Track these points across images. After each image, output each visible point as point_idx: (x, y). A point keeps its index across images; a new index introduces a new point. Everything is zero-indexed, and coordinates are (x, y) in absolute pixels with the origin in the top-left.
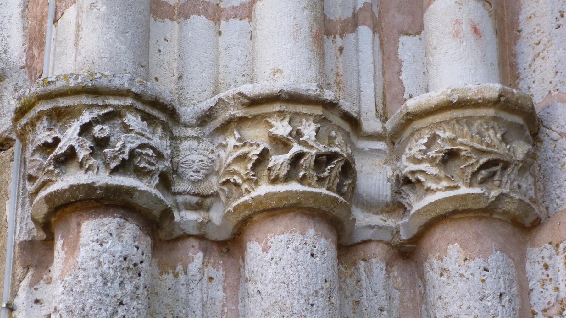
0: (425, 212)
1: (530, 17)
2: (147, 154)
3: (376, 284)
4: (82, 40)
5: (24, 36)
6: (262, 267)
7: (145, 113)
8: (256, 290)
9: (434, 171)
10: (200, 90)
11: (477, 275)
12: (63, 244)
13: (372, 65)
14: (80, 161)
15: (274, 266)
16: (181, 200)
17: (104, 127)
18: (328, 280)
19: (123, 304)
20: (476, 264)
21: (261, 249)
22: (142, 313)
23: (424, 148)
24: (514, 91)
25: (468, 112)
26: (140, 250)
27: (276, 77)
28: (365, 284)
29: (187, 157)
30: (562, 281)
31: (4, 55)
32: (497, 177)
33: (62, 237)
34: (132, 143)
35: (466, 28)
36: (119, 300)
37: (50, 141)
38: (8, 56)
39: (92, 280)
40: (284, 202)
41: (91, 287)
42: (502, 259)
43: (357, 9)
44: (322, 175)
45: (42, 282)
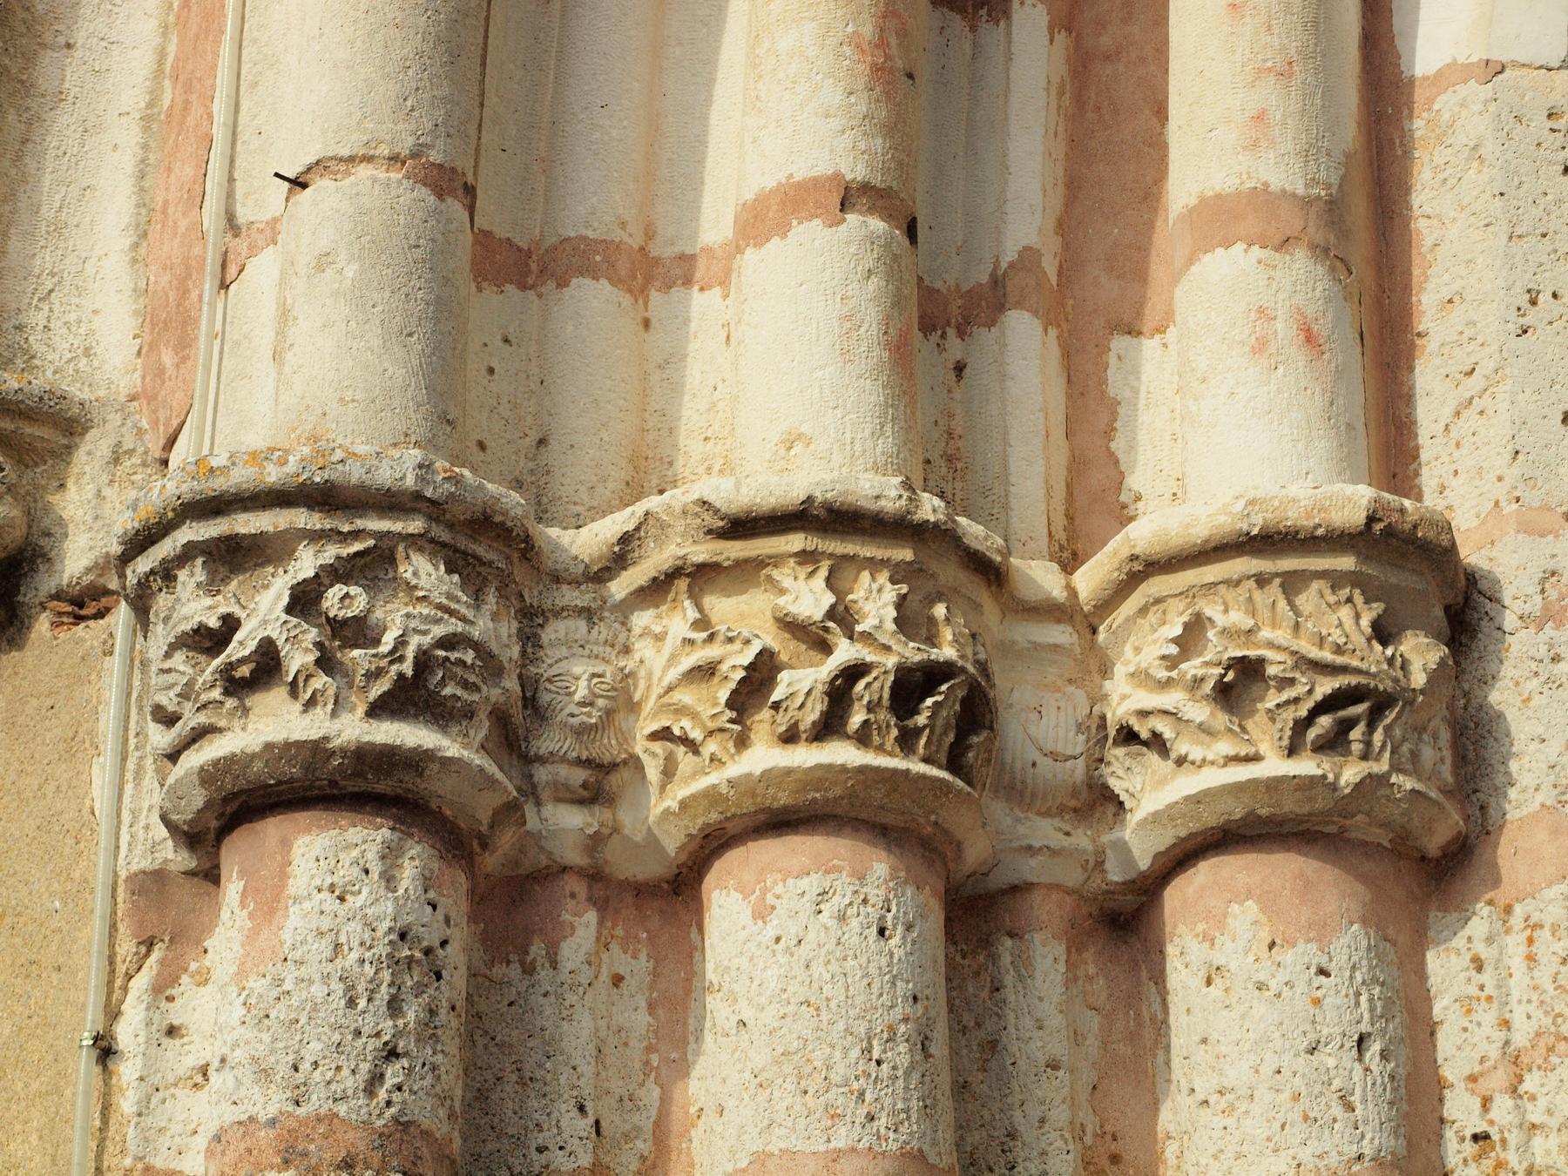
1: (1450, 301)
2: (461, 663)
3: (1041, 999)
4: (296, 349)
5: (136, 313)
6: (751, 959)
7: (456, 550)
8: (734, 1019)
9: (1199, 712)
11: (1301, 987)
12: (244, 895)
13: (1041, 414)
15: (783, 959)
16: (544, 778)
17: (354, 590)
18: (919, 995)
19: (397, 1056)
20: (1298, 957)
21: (749, 911)
22: (444, 1077)
24: (1407, 503)
27: (793, 452)
28: (1012, 998)
30: (1520, 1002)
31: (84, 361)
32: (1356, 734)
33: (242, 874)
34: (425, 633)
35: (1284, 329)
36: (386, 1044)
37: (213, 623)
38: (96, 364)
41: (315, 1009)
42: (1364, 943)
43: (1004, 265)
44: (910, 723)
45: (185, 979)
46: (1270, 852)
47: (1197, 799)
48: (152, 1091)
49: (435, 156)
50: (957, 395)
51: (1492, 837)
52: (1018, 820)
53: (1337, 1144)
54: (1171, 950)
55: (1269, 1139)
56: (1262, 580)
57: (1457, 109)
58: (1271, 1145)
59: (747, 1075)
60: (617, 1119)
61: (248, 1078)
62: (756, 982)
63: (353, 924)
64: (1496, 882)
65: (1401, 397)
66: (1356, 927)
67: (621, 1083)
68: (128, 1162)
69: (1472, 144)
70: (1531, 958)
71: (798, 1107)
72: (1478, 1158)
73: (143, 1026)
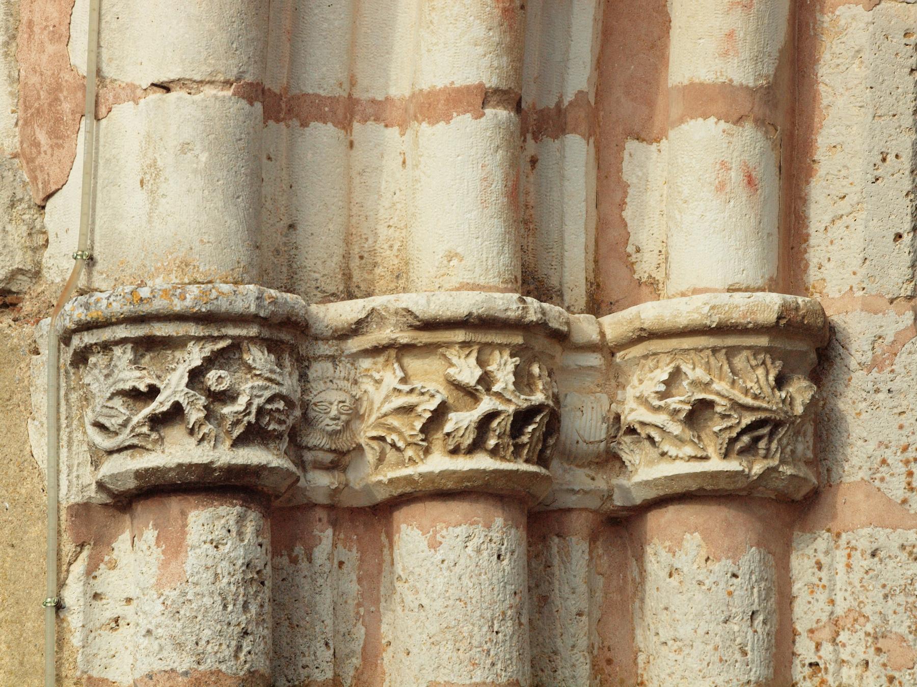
0: (656, 485)
1: (834, 147)
2: (278, 410)
3: (575, 576)
6: (427, 571)
8: (417, 603)
9: (676, 429)
10: (326, 256)
11: (722, 585)
12: (158, 538)
14: (190, 426)
15: (446, 574)
16: (310, 458)
21: (426, 543)
23: (662, 388)
25: (731, 341)
26: (264, 547)
27: (452, 263)
28: (557, 573)
29: (321, 395)
30: (841, 589)
32: (762, 444)
33: (156, 526)
34: (260, 396)
35: (735, 176)
37: (143, 388)
39: (207, 601)
40: (466, 484)
41: (206, 611)
42: (758, 558)
43: (566, 103)
45: (102, 566)
46: (709, 505)
47: (672, 478)
48: (88, 630)
49: (249, 78)
50: (532, 179)
51: (833, 489)
52: (565, 471)
53: (738, 674)
54: (649, 550)
55: (700, 671)
56: (715, 350)
57: (850, 20)
58: (701, 674)
59: (425, 636)
60: (342, 647)
61: (169, 647)
62: (430, 585)
63: (224, 563)
64: (834, 517)
65: (801, 198)
66: (754, 549)
67: (344, 625)
68: (78, 673)
69: (857, 48)
70: (849, 566)
71: (454, 659)
72: (811, 677)
73: (82, 595)
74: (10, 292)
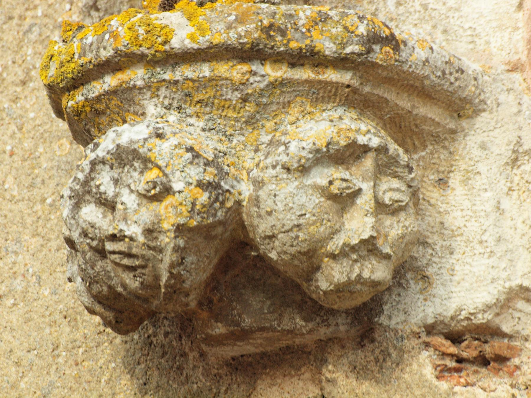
74: (498, 333)
